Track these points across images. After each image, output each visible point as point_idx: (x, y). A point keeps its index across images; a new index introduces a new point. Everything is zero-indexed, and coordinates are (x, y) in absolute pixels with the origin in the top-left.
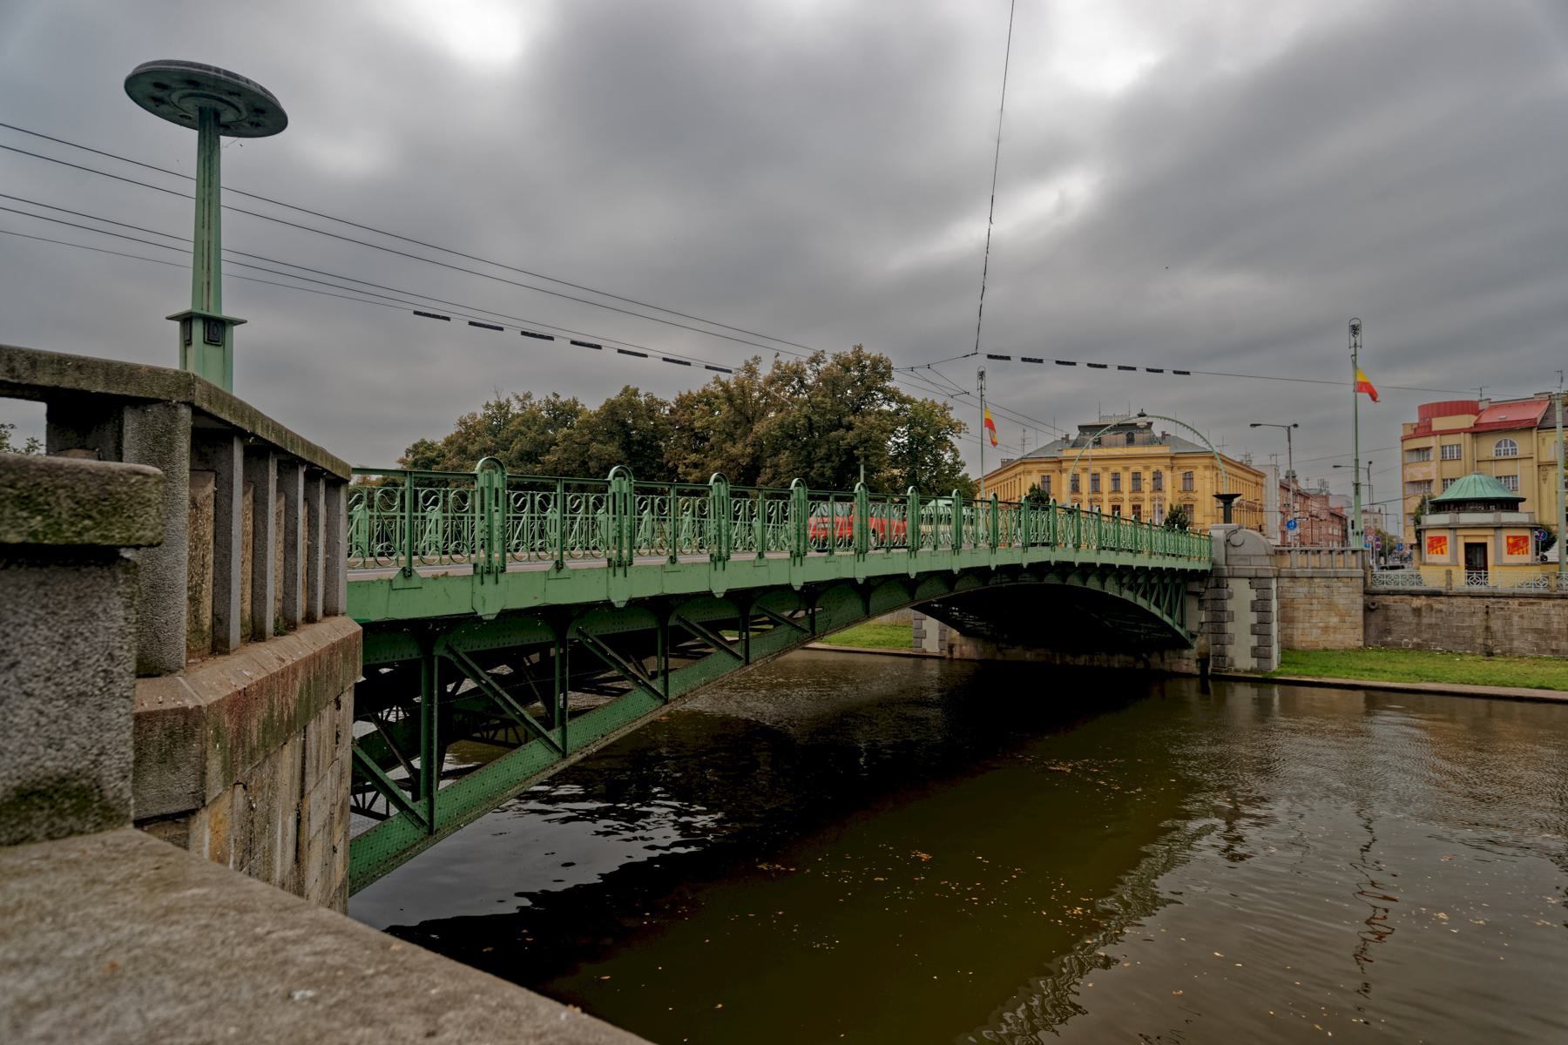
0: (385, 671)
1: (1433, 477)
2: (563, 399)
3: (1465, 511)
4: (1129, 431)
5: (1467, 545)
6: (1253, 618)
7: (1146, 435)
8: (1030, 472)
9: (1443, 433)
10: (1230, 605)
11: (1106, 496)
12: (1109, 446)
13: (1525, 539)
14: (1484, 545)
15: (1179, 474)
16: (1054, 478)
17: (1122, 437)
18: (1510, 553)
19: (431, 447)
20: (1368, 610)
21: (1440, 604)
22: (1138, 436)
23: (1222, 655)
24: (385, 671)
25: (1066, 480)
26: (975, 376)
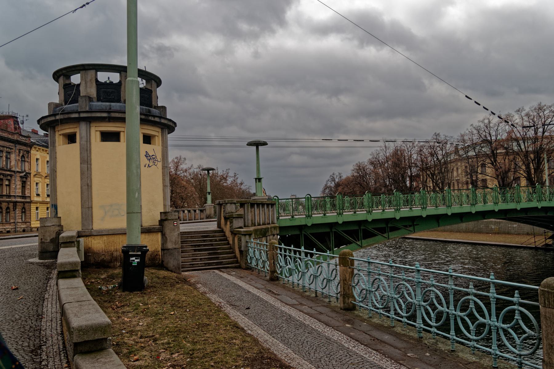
0: (428, 354)
24: (428, 354)
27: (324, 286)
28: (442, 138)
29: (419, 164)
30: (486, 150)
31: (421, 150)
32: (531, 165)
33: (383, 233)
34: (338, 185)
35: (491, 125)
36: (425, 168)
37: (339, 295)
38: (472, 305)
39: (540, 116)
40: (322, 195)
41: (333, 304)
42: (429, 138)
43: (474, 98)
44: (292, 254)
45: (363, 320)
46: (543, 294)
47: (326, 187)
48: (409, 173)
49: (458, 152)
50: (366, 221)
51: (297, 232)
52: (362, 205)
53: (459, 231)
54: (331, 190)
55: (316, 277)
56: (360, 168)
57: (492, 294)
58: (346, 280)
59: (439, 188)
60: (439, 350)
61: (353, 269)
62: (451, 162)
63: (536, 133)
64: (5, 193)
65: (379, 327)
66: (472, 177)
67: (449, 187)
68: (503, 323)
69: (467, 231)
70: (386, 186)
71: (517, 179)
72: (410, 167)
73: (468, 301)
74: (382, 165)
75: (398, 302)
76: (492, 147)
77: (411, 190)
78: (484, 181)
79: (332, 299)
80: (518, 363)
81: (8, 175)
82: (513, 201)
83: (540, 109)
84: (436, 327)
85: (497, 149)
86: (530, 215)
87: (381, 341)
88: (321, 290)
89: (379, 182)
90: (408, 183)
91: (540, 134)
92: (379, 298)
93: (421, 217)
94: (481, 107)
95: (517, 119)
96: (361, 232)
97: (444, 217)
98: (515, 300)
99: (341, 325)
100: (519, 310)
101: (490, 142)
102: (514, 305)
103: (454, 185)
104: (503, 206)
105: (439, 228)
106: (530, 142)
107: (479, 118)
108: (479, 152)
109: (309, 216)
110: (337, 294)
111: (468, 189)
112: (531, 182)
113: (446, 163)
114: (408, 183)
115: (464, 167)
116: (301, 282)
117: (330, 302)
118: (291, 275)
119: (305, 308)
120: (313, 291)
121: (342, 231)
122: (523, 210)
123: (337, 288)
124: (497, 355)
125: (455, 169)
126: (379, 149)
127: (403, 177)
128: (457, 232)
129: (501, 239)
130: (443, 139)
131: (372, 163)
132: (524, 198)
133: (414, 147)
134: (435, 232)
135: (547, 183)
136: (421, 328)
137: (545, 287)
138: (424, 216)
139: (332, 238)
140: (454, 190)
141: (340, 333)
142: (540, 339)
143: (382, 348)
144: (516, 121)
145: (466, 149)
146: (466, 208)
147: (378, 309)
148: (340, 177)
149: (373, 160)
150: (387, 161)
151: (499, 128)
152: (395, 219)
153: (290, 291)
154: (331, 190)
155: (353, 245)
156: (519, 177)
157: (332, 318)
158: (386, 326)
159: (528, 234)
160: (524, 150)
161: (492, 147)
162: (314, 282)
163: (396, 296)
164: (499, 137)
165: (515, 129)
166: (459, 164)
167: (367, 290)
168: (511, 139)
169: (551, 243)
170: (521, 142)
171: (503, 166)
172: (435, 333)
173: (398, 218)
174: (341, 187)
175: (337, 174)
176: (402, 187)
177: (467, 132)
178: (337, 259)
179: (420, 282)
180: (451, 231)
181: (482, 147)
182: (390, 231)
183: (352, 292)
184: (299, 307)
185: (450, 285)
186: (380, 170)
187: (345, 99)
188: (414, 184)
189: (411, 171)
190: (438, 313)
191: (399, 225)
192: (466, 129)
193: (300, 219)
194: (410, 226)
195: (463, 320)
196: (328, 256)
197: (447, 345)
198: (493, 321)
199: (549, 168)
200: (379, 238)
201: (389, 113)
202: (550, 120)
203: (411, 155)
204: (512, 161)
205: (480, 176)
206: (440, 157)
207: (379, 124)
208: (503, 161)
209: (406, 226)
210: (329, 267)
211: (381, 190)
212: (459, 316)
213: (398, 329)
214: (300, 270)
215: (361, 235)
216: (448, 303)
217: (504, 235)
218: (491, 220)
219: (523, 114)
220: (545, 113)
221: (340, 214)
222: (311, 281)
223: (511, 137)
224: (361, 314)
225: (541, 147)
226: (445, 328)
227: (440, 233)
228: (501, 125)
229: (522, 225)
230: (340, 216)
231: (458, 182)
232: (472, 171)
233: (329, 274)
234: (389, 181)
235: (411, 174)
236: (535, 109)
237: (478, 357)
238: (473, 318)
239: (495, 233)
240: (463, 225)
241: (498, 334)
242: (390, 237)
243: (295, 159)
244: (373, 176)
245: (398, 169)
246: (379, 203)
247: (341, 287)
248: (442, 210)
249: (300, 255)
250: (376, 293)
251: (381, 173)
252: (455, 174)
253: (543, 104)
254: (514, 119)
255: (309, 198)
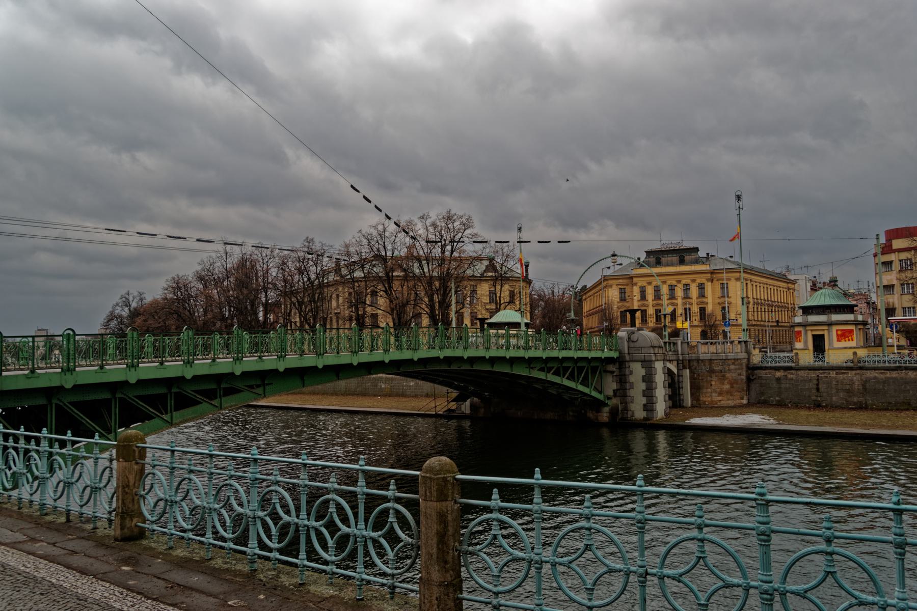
0: (262, 597)
1: (895, 282)
3: (812, 314)
4: (683, 255)
5: (814, 336)
6: (643, 386)
7: (693, 256)
8: (611, 286)
9: (900, 250)
10: (632, 379)
11: (679, 301)
12: (667, 265)
13: (851, 331)
14: (823, 336)
15: (717, 285)
16: (628, 289)
17: (675, 259)
18: (839, 340)
20: (749, 380)
21: (791, 375)
22: (687, 258)
23: (626, 409)
24: (262, 597)
25: (636, 290)
26: (734, 198)
27: (85, 500)
28: (317, 246)
29: (280, 284)
30: (379, 270)
31: (284, 263)
32: (436, 296)
33: (212, 399)
34: (135, 314)
35: (387, 234)
36: (288, 292)
37: (113, 514)
38: (332, 509)
39: (449, 229)
40: (103, 332)
41: (100, 532)
42: (298, 245)
43: (363, 192)
44: (22, 444)
45: (156, 555)
46: (424, 483)
47: (112, 317)
48: (263, 300)
49: (340, 269)
50: (182, 378)
51: (41, 401)
52: (176, 351)
53: (335, 393)
54: (122, 322)
55: (68, 485)
56: (178, 285)
57: (361, 488)
58: (128, 486)
59: (309, 324)
60: (281, 586)
61: (144, 464)
62: (329, 285)
63: (443, 252)
65: (184, 564)
66: (357, 309)
67: (324, 325)
68: (316, 521)
69: (347, 393)
70: (223, 319)
71: (417, 316)
72: (265, 290)
73: (386, 512)
74: (218, 282)
75: (220, 515)
76: (386, 267)
77: (265, 327)
78: (375, 317)
79: (99, 524)
80: (389, 587)
82: (409, 348)
83: (449, 218)
84: (232, 540)
85: (393, 271)
86: (431, 368)
87: (185, 587)
88: (78, 509)
89: (212, 311)
90: (261, 315)
91: (447, 254)
92: (188, 512)
93: (276, 371)
94: (372, 205)
95: (420, 229)
96: (170, 399)
97: (310, 372)
98: (389, 494)
99: (113, 569)
100: (394, 509)
101: (384, 260)
102: (389, 501)
103: (331, 320)
104: (395, 355)
105: (305, 389)
106: (435, 263)
107: (370, 221)
108: (369, 272)
109: (68, 370)
110: (110, 513)
111: (350, 329)
112: (434, 321)
113: (321, 286)
114: (261, 315)
115: (347, 295)
116: (36, 498)
117: (96, 528)
118: (15, 486)
119: (41, 547)
120: (61, 513)
121: (135, 397)
122: (423, 361)
123: (111, 502)
124: (363, 580)
125: (334, 296)
126: (214, 255)
127: (252, 304)
128: (332, 394)
129: (393, 404)
130: (318, 248)
131: (201, 279)
132: (425, 346)
133: (274, 257)
134: (300, 396)
135: (454, 325)
136: (255, 554)
137: (426, 473)
138: (281, 369)
139: (116, 410)
140: (331, 329)
141: (108, 585)
142: (419, 548)
143: (185, 600)
144: (420, 232)
145: (351, 266)
146: (346, 358)
147: (185, 531)
148: (141, 300)
149: (203, 273)
150: (228, 277)
151: (397, 240)
152: (232, 374)
153: (10, 516)
154: (122, 322)
155: (156, 422)
156: (420, 314)
157: (96, 558)
158: (197, 559)
159: (427, 396)
160: (427, 275)
161: (386, 267)
162: (92, 500)
163: (216, 506)
164: (396, 253)
165: (417, 244)
166: (341, 289)
167: (166, 501)
168: (411, 257)
169: (454, 408)
170: (424, 262)
171: (400, 296)
172: (277, 559)
173: (238, 373)
174: (142, 318)
175: (136, 294)
176: (250, 322)
177: (354, 240)
178: (114, 451)
179: (257, 479)
180: (324, 393)
181: (374, 266)
182: (224, 396)
183: (139, 506)
184: (29, 546)
185: (303, 480)
186: (215, 291)
187: (147, 159)
188: (271, 317)
189: (266, 296)
190: (342, 536)
191: (240, 385)
192: (350, 236)
193: (49, 374)
194: (258, 386)
195: (319, 534)
196: (97, 444)
197: (293, 576)
198: (360, 530)
199: (457, 302)
200: (204, 406)
201: (227, 195)
202: (460, 235)
203: (267, 270)
204: (411, 289)
205: (368, 309)
206: (313, 277)
207: (210, 212)
208: (400, 289)
209: (251, 387)
210: (96, 464)
211: (215, 325)
212: (313, 527)
213: (218, 563)
214: (36, 473)
215: (171, 403)
216: (298, 509)
217: (397, 399)
218: (381, 375)
219: (428, 222)
220: (455, 224)
221: (133, 366)
222: (59, 494)
223: (412, 254)
224: (153, 545)
225: (448, 273)
226: (291, 549)
227: (307, 397)
228: (399, 235)
229: (421, 382)
230: (133, 370)
231: (337, 317)
232: (357, 302)
233: (95, 477)
234: (230, 311)
235: (267, 301)
236: (444, 218)
237: (337, 588)
238: (332, 527)
239: (385, 396)
240: (342, 384)
241: (366, 546)
242: (224, 405)
243: (45, 259)
244: (201, 300)
245: (245, 291)
246: (207, 348)
247: (117, 501)
248: (310, 360)
249: (38, 444)
250: (183, 504)
251: (216, 297)
252: (334, 304)
253: (453, 212)
254: (417, 229)
255: (70, 336)
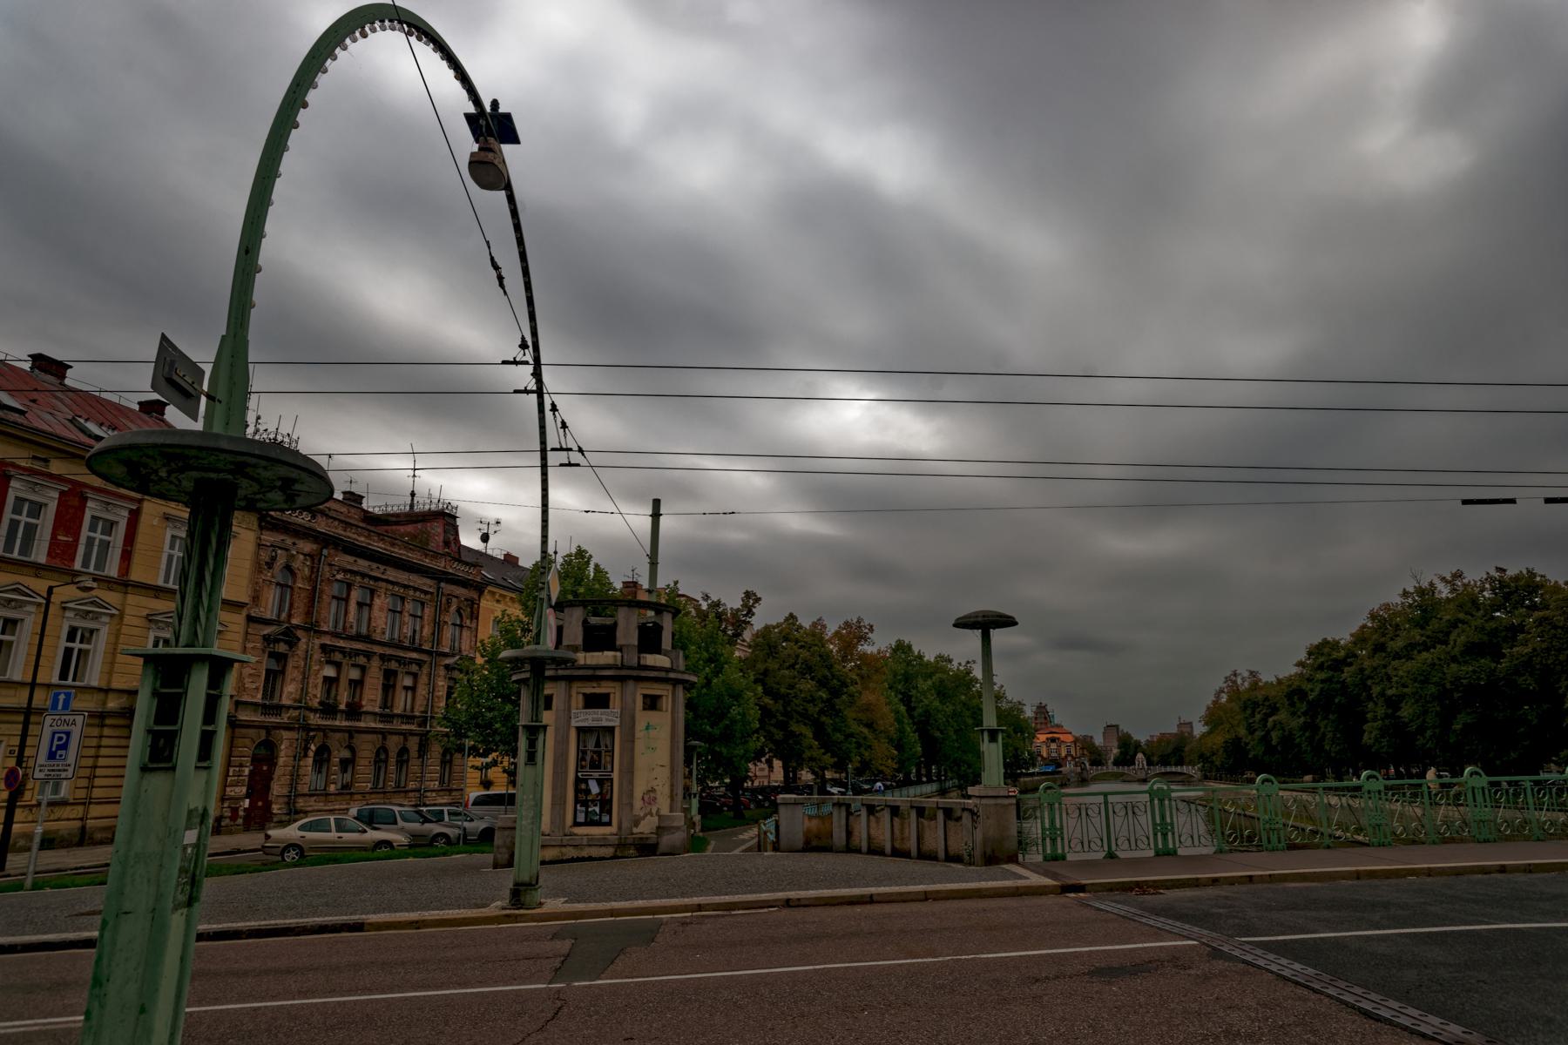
2: (1511, 572)
19: (1335, 645)
64: (398, 711)
81: (412, 661)
